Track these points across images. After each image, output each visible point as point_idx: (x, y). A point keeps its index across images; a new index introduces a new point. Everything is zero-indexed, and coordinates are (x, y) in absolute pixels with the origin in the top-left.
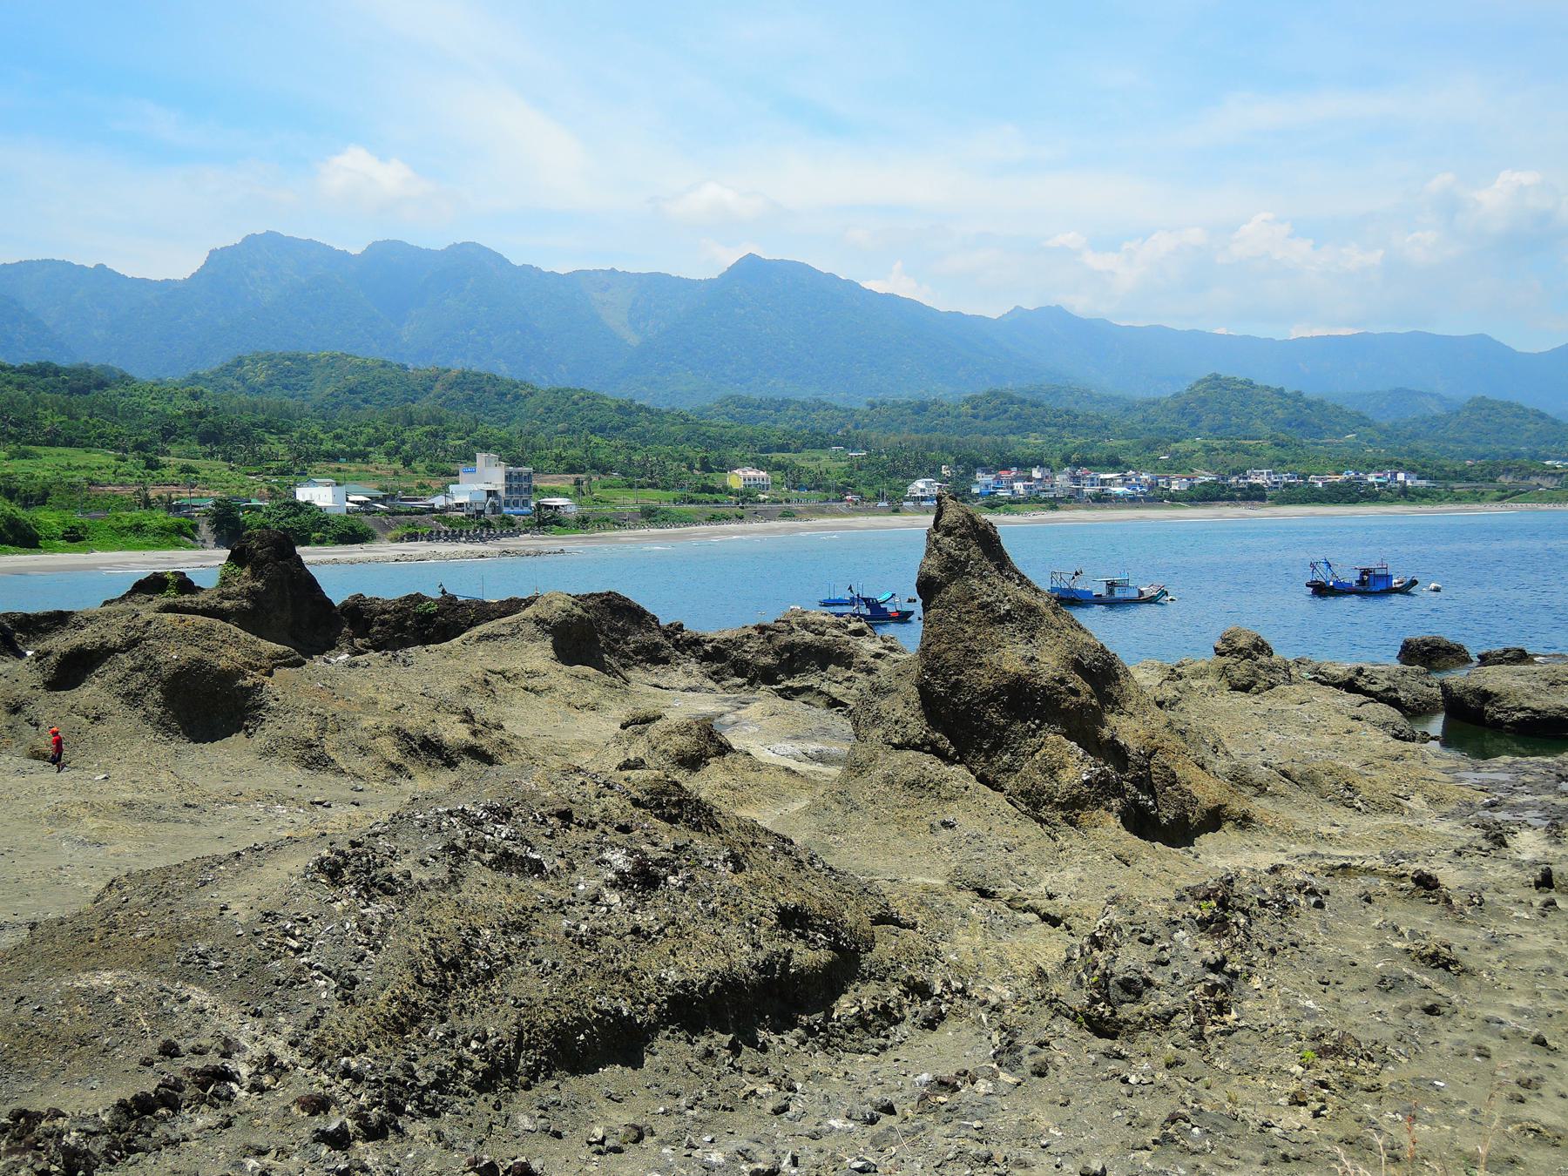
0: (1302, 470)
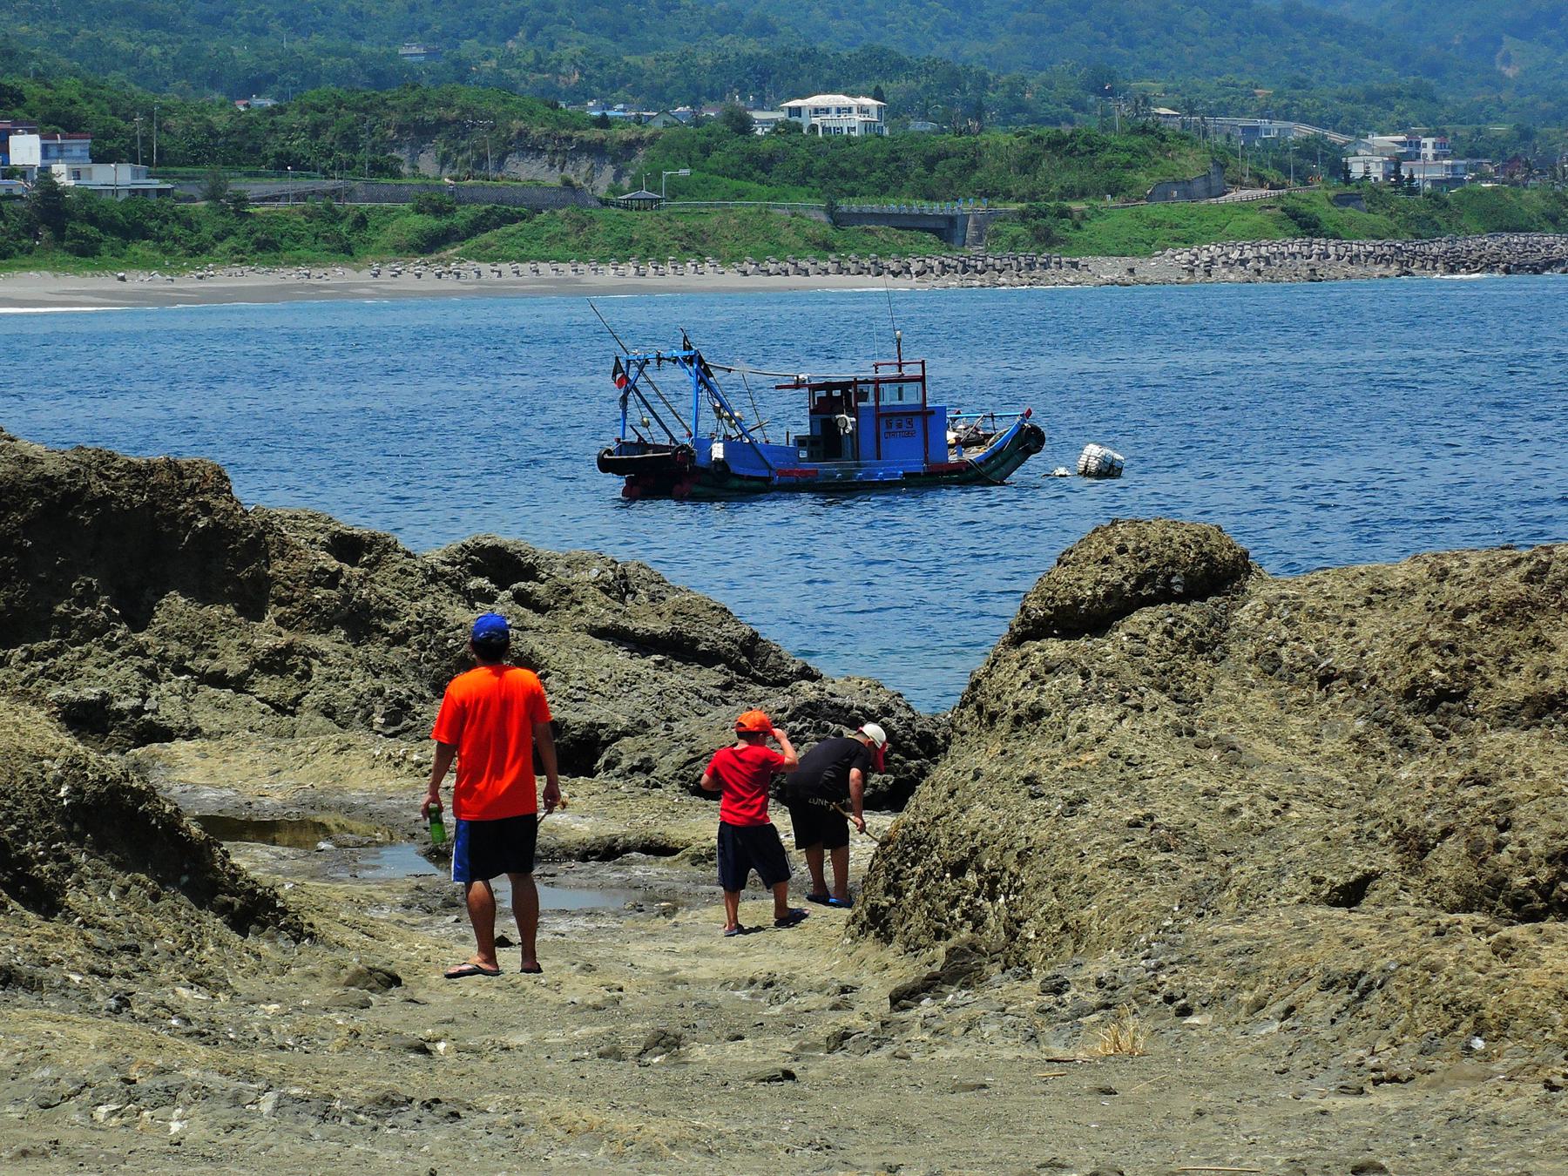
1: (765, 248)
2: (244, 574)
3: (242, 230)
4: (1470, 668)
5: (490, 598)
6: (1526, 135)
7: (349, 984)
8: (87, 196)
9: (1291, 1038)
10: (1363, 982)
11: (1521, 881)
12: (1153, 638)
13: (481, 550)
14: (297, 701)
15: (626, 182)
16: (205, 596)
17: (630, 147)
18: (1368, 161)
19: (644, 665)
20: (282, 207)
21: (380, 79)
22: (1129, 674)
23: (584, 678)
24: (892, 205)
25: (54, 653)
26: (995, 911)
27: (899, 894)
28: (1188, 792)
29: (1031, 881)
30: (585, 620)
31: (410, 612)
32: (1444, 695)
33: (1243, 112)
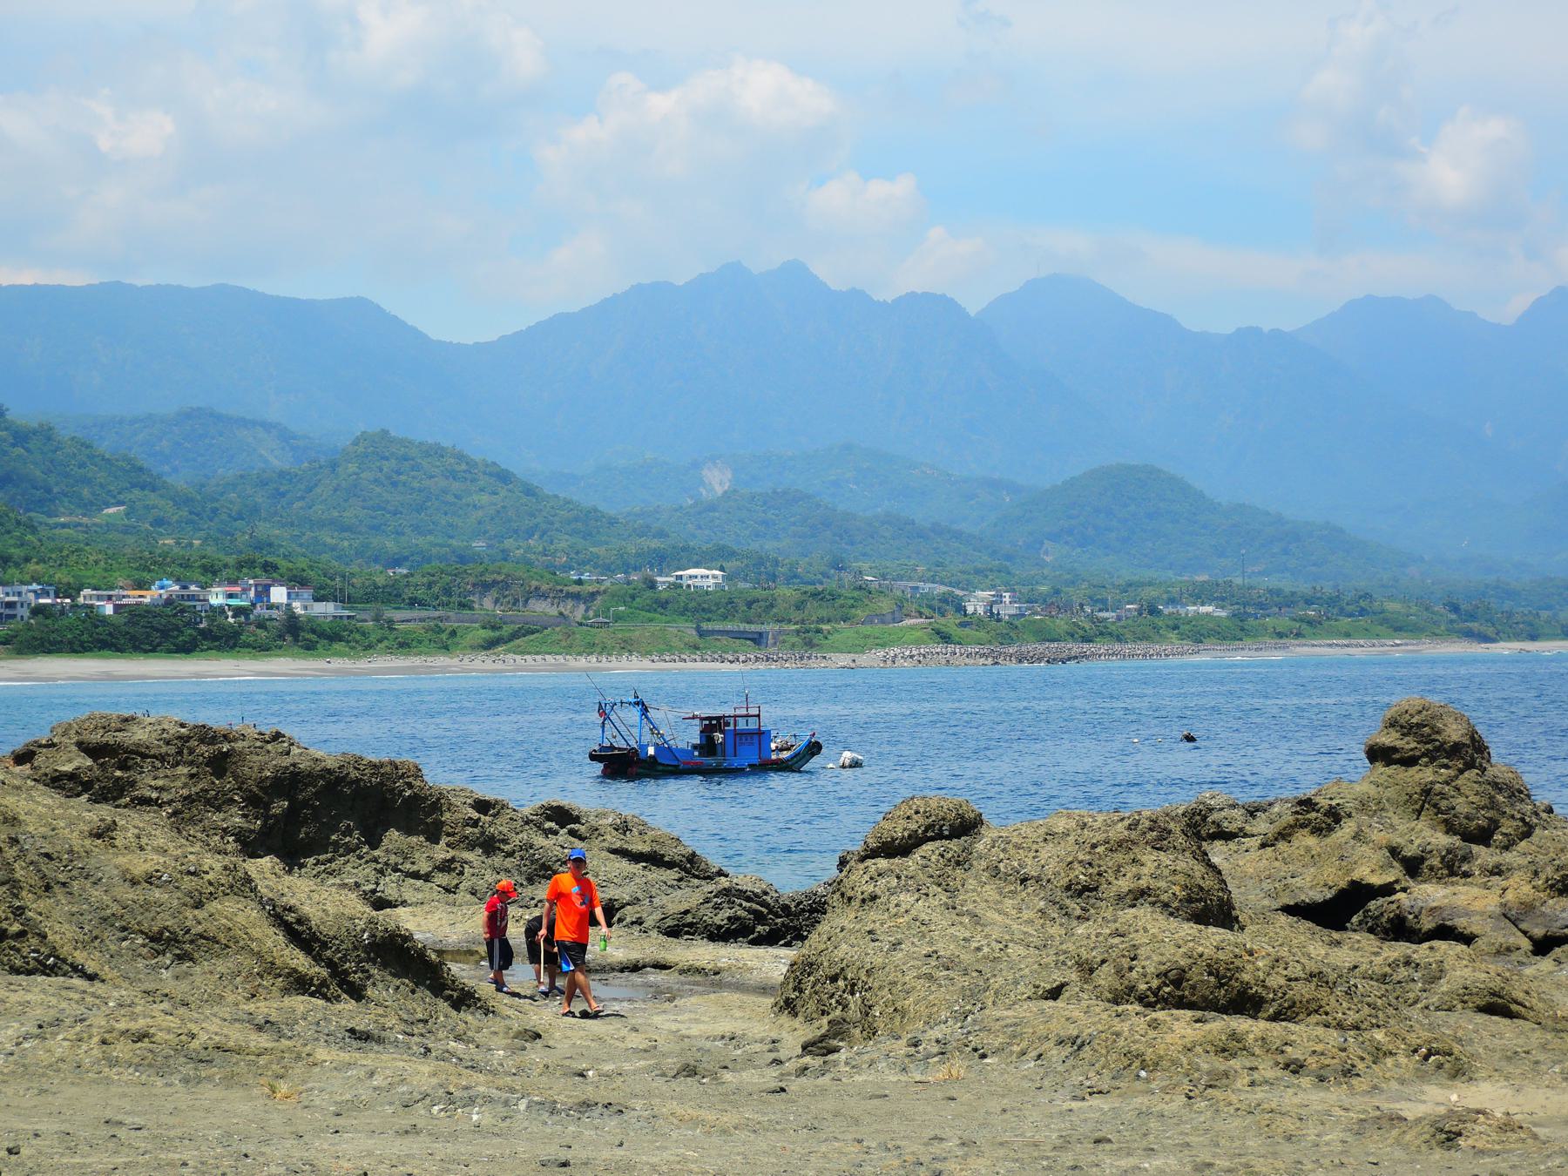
0: (62, 576)
1: (664, 648)
2: (429, 820)
3: (392, 637)
4: (1100, 874)
5: (556, 833)
6: (1057, 592)
7: (515, 1037)
8: (311, 619)
9: (1042, 1070)
10: (1079, 1041)
11: (1143, 987)
12: (934, 858)
13: (551, 808)
14: (457, 886)
15: (591, 613)
16: (409, 832)
17: (593, 595)
18: (976, 604)
19: (637, 868)
20: (411, 625)
21: (462, 559)
22: (921, 876)
23: (613, 877)
24: (729, 627)
25: (330, 861)
26: (854, 1001)
27: (801, 991)
28: (954, 938)
29: (876, 985)
30: (606, 844)
31: (516, 840)
32: (1086, 889)
33: (910, 579)
